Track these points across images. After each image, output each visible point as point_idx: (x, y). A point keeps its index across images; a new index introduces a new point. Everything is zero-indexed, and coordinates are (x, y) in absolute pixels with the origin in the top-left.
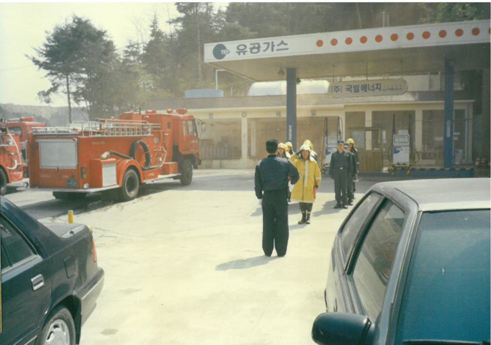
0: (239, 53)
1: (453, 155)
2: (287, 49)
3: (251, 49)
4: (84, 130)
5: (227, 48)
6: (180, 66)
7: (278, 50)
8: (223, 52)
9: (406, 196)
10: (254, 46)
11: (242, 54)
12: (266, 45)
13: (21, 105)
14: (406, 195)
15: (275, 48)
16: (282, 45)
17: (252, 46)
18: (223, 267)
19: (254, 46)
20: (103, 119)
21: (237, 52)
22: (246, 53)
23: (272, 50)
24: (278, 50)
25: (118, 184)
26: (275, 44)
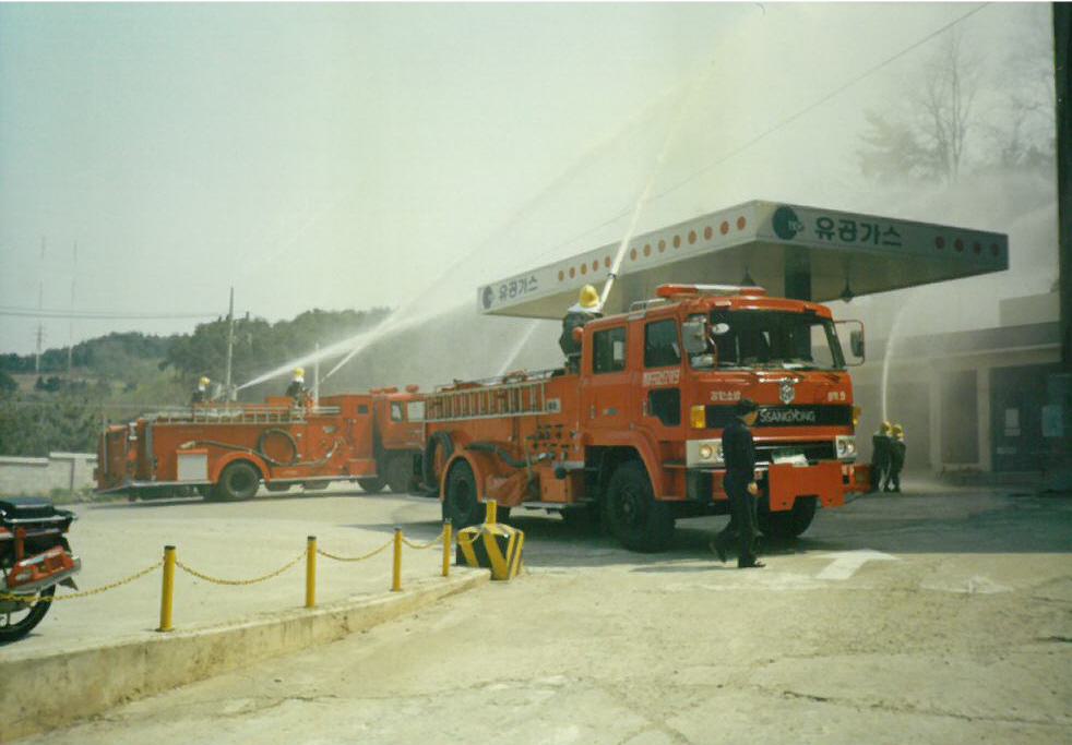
0: (821, 235)
1: (825, 586)
2: (899, 244)
3: (842, 231)
4: (238, 316)
5: (800, 220)
6: (327, 431)
7: (886, 243)
8: (792, 225)
9: (347, 557)
10: (846, 227)
11: (825, 237)
12: (866, 230)
13: (77, 344)
14: (349, 560)
15: (881, 238)
16: (892, 235)
17: (842, 226)
18: (232, 289)
19: (846, 227)
20: (31, 591)
21: (817, 232)
22: (833, 237)
23: (876, 243)
24: (886, 243)
25: (210, 477)
26: (880, 229)
